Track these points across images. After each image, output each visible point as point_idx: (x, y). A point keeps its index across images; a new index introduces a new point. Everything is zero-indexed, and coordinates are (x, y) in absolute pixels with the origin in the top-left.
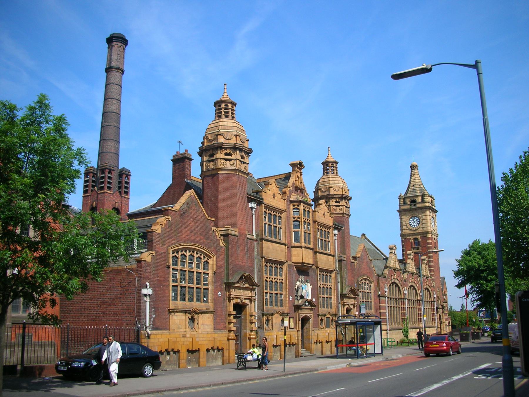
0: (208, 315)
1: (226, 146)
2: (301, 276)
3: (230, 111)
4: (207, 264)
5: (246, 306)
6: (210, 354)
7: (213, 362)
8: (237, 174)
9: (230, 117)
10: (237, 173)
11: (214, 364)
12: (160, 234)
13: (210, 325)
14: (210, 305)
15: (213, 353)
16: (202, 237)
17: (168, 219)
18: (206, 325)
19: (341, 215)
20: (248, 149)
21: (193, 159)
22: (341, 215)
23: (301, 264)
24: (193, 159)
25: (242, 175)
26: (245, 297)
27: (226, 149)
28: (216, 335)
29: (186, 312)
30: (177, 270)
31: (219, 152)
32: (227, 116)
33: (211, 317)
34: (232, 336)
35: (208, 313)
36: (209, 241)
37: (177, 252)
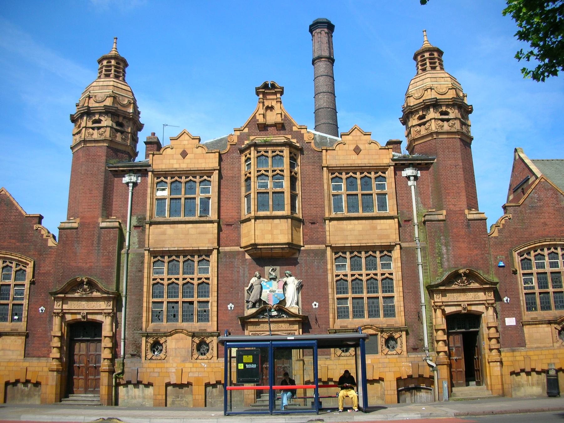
0: (13, 337)
1: (76, 116)
2: (266, 268)
3: (437, 60)
4: (24, 272)
5: (481, 315)
6: (18, 390)
7: (23, 400)
8: (435, 138)
9: (438, 68)
10: (435, 137)
11: (31, 402)
12: (497, 237)
13: (17, 350)
14: (22, 326)
15: (23, 388)
16: (14, 241)
17: (507, 218)
18: (10, 350)
19: (430, 138)
20: (451, 100)
21: (402, 141)
22: (430, 138)
23: (250, 248)
24: (402, 141)
25: (93, 145)
26: (469, 303)
27: (417, 111)
28: (26, 364)
29: (549, 323)
30: (531, 274)
31: (411, 119)
32: (433, 68)
33: (20, 340)
34: (105, 366)
35: (13, 335)
36: (25, 244)
37: (529, 254)
